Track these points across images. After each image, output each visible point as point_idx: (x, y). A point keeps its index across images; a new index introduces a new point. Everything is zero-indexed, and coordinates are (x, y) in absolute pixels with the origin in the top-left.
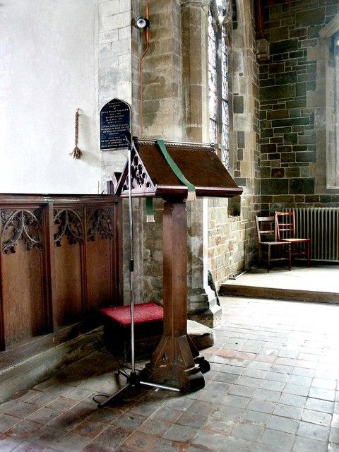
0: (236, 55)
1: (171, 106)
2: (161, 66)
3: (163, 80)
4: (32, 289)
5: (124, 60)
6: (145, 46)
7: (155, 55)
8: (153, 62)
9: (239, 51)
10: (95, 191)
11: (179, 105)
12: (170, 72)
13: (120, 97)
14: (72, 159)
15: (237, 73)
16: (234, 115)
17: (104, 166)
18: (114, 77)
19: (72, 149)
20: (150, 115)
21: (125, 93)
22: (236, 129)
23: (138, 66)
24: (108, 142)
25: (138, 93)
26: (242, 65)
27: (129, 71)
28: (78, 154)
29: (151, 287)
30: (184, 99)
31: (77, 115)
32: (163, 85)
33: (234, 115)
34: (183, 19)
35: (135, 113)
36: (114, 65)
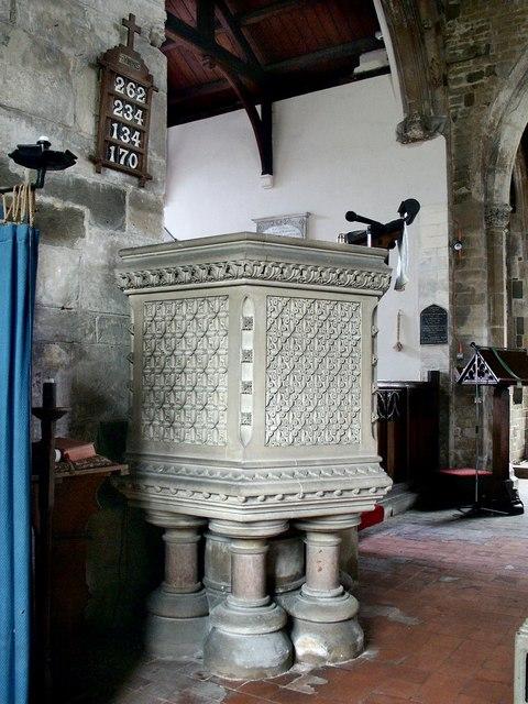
0: (515, 240)
1: (480, 311)
2: (471, 279)
3: (474, 290)
4: (26, 577)
5: (442, 273)
6: (457, 263)
7: (466, 269)
8: (464, 275)
9: (518, 235)
10: (418, 379)
11: (485, 311)
12: (479, 283)
13: (438, 303)
14: (395, 353)
15: (516, 258)
16: (514, 300)
17: (424, 357)
18: (434, 286)
19: (395, 342)
20: (461, 317)
21: (443, 300)
22: (515, 315)
23: (452, 278)
24: (426, 339)
25: (453, 300)
26: (521, 250)
27: (447, 283)
28: (399, 347)
29: (461, 459)
30: (489, 305)
31: (399, 315)
32: (474, 294)
33: (514, 300)
34: (488, 240)
35: (450, 316)
36: (433, 277)
